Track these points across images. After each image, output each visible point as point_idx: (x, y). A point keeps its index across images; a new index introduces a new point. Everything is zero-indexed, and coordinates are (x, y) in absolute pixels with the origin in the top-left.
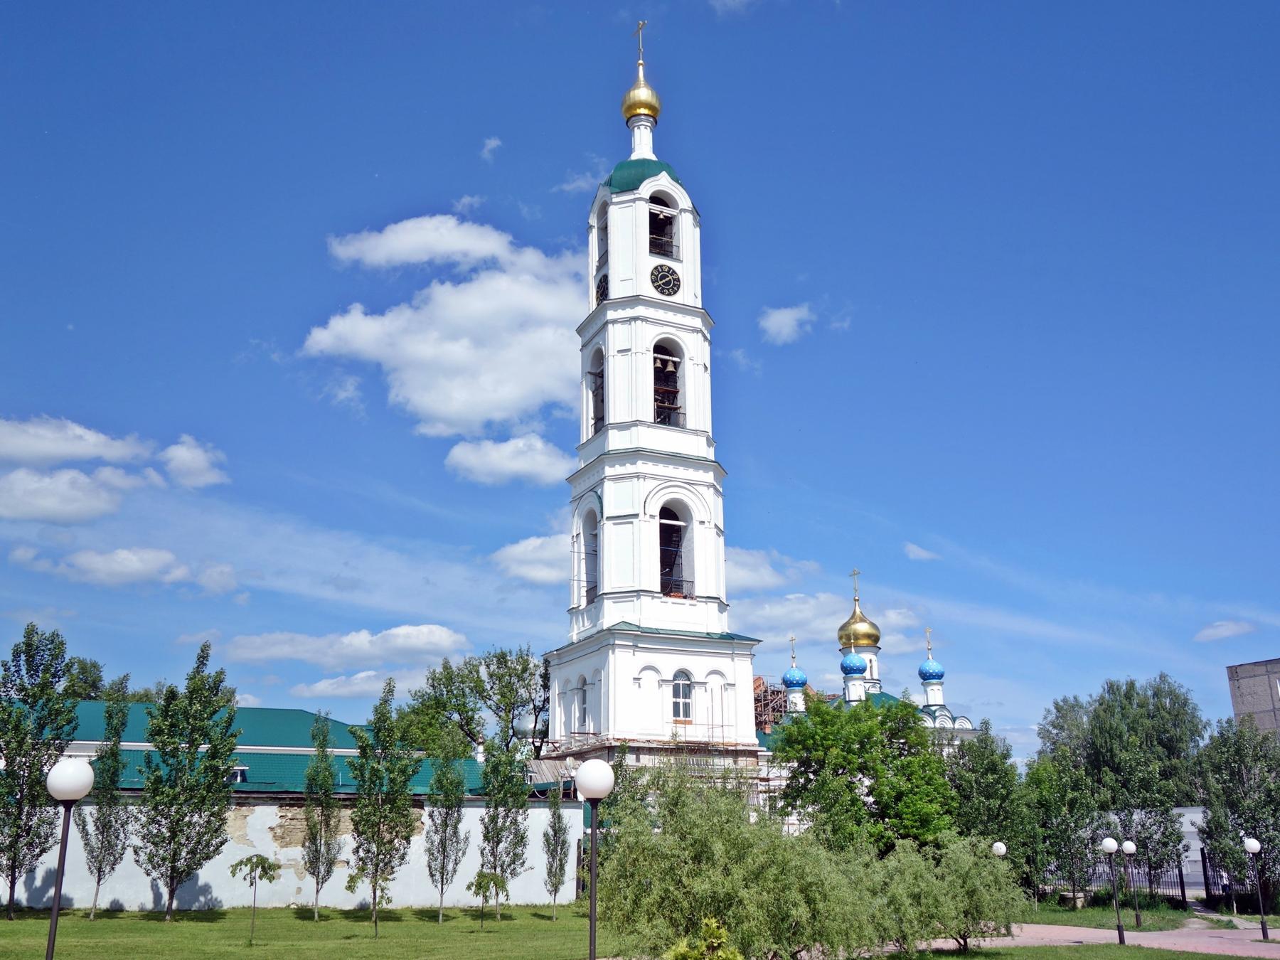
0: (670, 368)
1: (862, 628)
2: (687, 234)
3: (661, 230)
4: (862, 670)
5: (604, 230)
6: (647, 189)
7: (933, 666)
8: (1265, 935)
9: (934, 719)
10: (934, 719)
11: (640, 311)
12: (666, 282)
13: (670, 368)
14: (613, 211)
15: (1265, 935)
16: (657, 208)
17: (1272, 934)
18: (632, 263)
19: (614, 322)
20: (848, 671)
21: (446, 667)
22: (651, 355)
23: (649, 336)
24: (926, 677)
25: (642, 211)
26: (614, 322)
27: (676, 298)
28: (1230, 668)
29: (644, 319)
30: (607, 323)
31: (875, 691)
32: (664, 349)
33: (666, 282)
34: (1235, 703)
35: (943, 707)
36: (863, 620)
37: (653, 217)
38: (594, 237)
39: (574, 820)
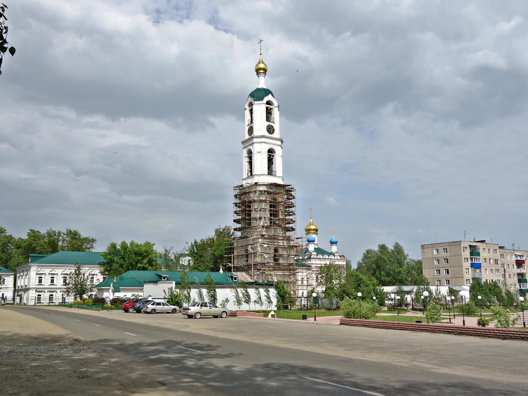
0: (272, 157)
1: (313, 227)
2: (276, 113)
3: (269, 112)
4: (313, 241)
5: (251, 111)
6: (266, 99)
7: (334, 240)
8: (524, 326)
9: (335, 256)
10: (335, 256)
11: (264, 140)
12: (271, 130)
13: (272, 157)
14: (255, 107)
15: (524, 326)
16: (268, 106)
17: (526, 326)
18: (260, 125)
19: (256, 143)
20: (309, 241)
21: (196, 242)
22: (267, 153)
23: (267, 147)
24: (332, 243)
25: (264, 107)
26: (256, 143)
27: (273, 136)
28: (422, 245)
29: (265, 143)
30: (253, 143)
31: (316, 247)
32: (271, 151)
33: (271, 130)
34: (422, 256)
35: (337, 252)
36: (313, 225)
37: (267, 108)
38: (247, 113)
39: (273, 292)
